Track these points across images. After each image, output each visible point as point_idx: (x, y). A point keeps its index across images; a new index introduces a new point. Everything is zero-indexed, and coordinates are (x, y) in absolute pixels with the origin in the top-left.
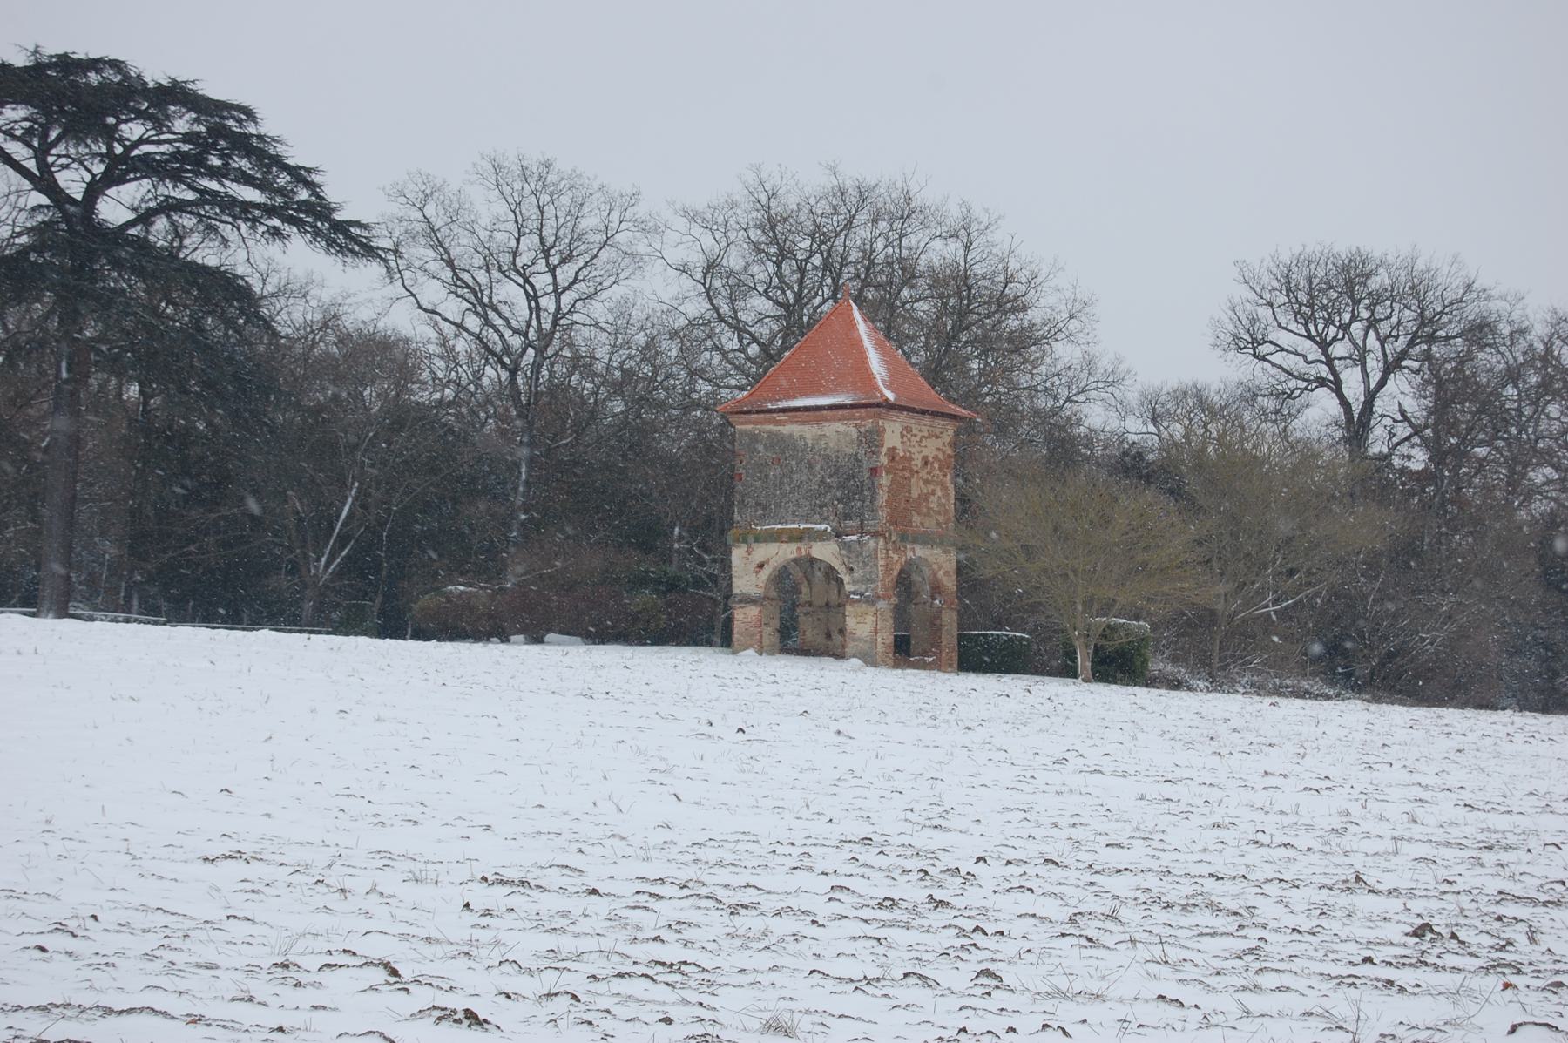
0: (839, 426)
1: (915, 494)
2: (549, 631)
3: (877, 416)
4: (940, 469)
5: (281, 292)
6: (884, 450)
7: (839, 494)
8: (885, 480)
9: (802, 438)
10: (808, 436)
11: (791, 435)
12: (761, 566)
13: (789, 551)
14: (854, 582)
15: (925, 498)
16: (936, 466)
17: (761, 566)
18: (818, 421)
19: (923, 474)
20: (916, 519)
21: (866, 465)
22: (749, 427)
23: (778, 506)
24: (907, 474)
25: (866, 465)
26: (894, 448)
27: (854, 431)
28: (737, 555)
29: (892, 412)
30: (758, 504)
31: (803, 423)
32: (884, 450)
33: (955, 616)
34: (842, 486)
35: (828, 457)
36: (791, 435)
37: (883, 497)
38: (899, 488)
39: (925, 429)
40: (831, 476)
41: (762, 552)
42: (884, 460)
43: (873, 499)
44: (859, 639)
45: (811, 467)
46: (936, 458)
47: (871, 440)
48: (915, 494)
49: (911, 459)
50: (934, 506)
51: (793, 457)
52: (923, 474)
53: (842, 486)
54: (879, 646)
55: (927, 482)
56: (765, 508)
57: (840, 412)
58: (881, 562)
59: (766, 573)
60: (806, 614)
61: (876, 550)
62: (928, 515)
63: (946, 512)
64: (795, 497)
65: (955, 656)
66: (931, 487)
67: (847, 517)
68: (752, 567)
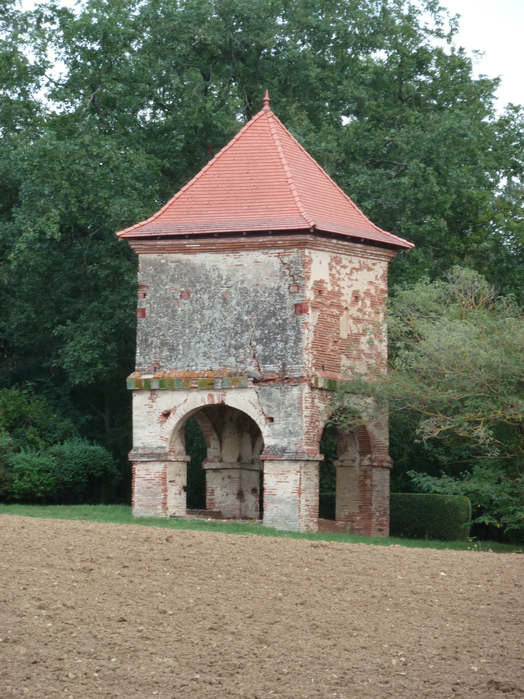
0: (259, 256)
1: (344, 335)
2: (126, 457)
3: (302, 245)
4: (373, 305)
5: (374, 447)
6: (310, 284)
7: (258, 333)
8: (311, 318)
9: (216, 269)
10: (222, 266)
11: (203, 266)
12: (167, 415)
13: (199, 399)
14: (275, 435)
15: (355, 339)
16: (368, 302)
17: (167, 415)
18: (235, 249)
19: (354, 311)
20: (344, 361)
21: (290, 302)
22: (153, 256)
23: (187, 345)
24: (336, 312)
25: (290, 302)
26: (322, 281)
27: (276, 262)
28: (139, 401)
29: (322, 240)
30: (163, 344)
31: (217, 251)
32: (310, 284)
33: (386, 474)
34: (261, 324)
35: (244, 292)
36: (203, 266)
37: (308, 337)
38: (325, 327)
39: (355, 259)
40: (248, 313)
41: (166, 400)
42: (310, 295)
43: (298, 340)
44: (281, 501)
45: (225, 301)
46: (367, 293)
47: (296, 278)
48: (344, 335)
49: (339, 294)
50: (365, 347)
51: (205, 290)
52: (354, 311)
53: (261, 324)
54: (303, 507)
55: (357, 320)
56: (172, 349)
57: (261, 240)
58: (306, 413)
59: (173, 421)
60: (216, 470)
61: (300, 398)
62: (359, 358)
63: (379, 355)
64: (206, 336)
65: (386, 520)
66: (361, 327)
67: (266, 359)
68: (157, 415)
